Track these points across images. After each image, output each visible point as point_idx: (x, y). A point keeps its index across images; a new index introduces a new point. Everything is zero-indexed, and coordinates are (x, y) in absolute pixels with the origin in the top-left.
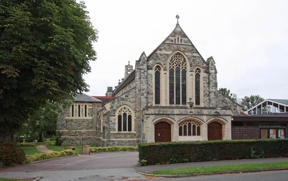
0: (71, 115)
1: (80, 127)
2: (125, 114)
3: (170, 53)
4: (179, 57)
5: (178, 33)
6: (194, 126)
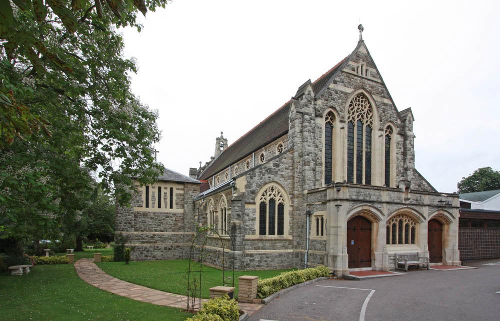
0: (144, 204)
1: (161, 227)
2: (272, 201)
3: (350, 92)
4: (362, 101)
5: (361, 56)
6: (407, 226)
